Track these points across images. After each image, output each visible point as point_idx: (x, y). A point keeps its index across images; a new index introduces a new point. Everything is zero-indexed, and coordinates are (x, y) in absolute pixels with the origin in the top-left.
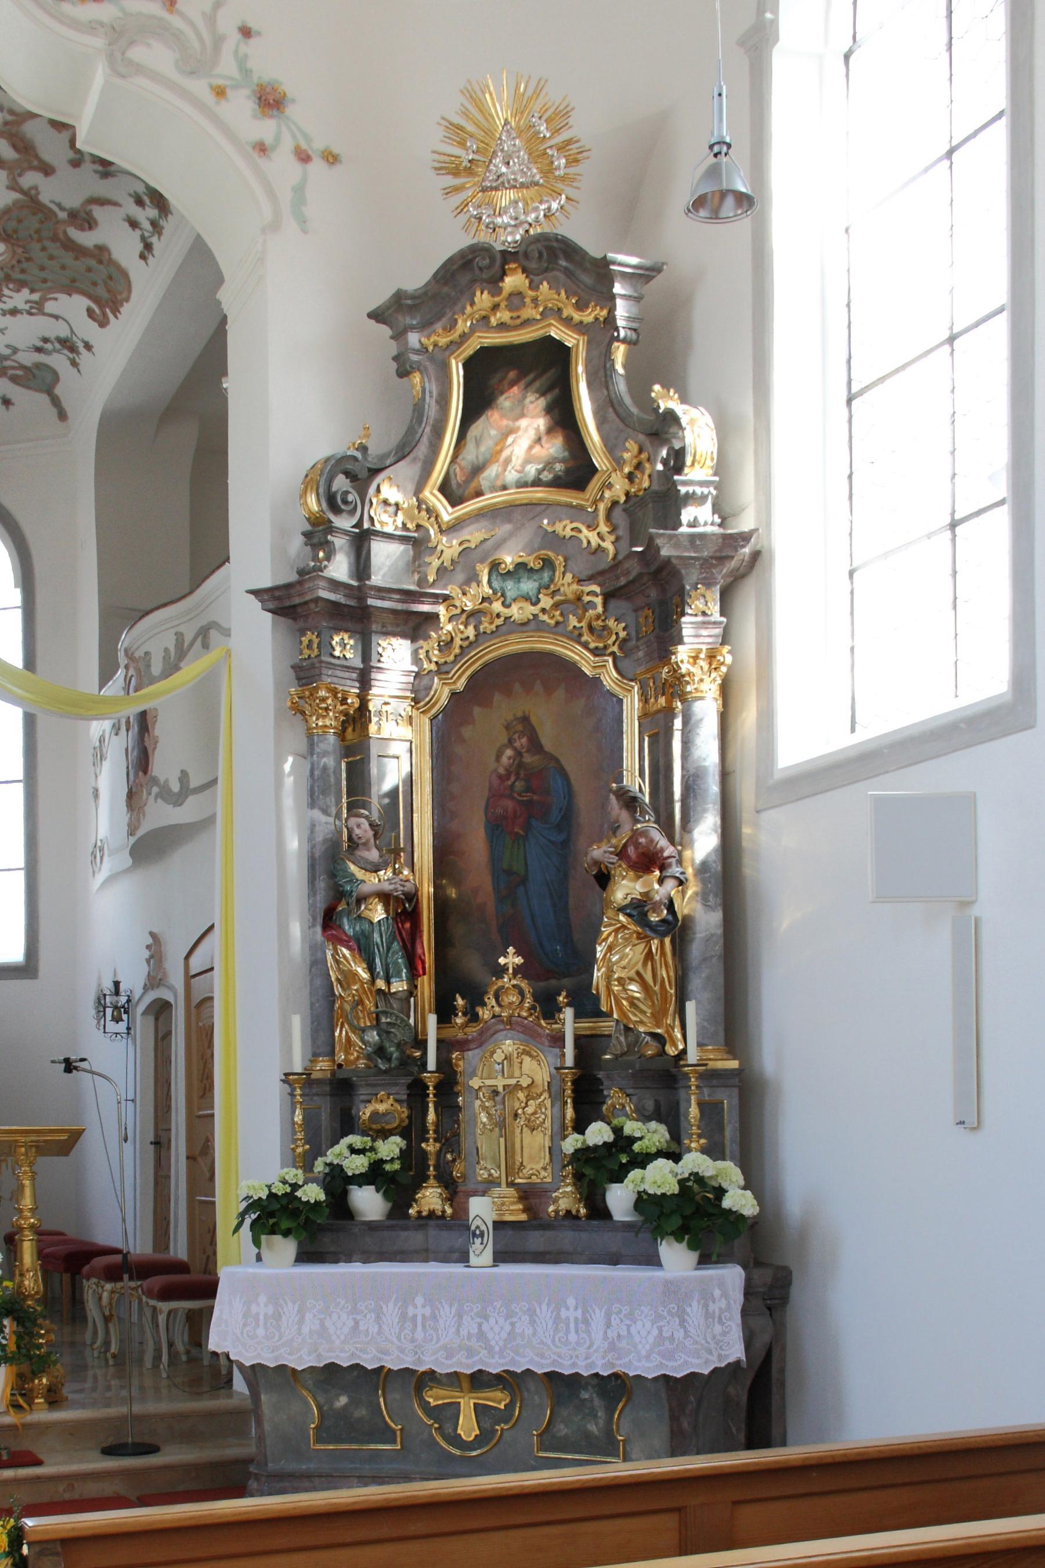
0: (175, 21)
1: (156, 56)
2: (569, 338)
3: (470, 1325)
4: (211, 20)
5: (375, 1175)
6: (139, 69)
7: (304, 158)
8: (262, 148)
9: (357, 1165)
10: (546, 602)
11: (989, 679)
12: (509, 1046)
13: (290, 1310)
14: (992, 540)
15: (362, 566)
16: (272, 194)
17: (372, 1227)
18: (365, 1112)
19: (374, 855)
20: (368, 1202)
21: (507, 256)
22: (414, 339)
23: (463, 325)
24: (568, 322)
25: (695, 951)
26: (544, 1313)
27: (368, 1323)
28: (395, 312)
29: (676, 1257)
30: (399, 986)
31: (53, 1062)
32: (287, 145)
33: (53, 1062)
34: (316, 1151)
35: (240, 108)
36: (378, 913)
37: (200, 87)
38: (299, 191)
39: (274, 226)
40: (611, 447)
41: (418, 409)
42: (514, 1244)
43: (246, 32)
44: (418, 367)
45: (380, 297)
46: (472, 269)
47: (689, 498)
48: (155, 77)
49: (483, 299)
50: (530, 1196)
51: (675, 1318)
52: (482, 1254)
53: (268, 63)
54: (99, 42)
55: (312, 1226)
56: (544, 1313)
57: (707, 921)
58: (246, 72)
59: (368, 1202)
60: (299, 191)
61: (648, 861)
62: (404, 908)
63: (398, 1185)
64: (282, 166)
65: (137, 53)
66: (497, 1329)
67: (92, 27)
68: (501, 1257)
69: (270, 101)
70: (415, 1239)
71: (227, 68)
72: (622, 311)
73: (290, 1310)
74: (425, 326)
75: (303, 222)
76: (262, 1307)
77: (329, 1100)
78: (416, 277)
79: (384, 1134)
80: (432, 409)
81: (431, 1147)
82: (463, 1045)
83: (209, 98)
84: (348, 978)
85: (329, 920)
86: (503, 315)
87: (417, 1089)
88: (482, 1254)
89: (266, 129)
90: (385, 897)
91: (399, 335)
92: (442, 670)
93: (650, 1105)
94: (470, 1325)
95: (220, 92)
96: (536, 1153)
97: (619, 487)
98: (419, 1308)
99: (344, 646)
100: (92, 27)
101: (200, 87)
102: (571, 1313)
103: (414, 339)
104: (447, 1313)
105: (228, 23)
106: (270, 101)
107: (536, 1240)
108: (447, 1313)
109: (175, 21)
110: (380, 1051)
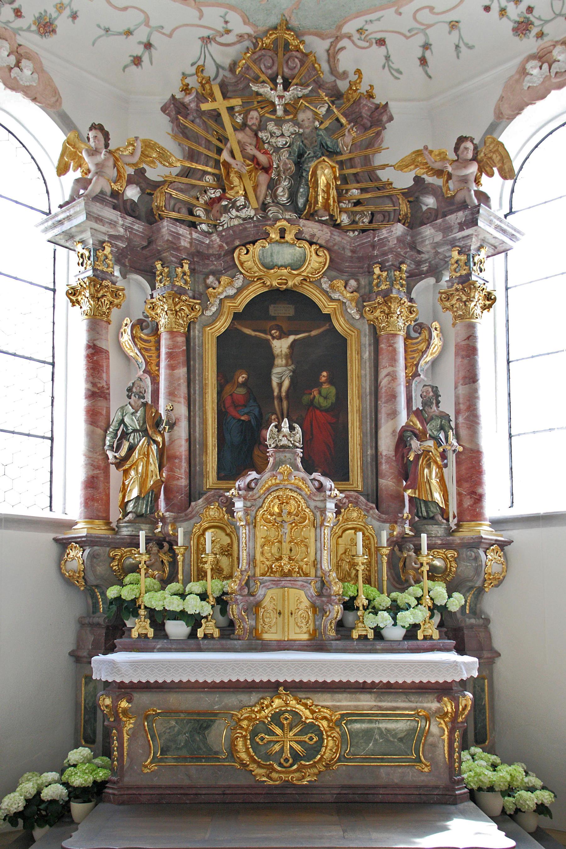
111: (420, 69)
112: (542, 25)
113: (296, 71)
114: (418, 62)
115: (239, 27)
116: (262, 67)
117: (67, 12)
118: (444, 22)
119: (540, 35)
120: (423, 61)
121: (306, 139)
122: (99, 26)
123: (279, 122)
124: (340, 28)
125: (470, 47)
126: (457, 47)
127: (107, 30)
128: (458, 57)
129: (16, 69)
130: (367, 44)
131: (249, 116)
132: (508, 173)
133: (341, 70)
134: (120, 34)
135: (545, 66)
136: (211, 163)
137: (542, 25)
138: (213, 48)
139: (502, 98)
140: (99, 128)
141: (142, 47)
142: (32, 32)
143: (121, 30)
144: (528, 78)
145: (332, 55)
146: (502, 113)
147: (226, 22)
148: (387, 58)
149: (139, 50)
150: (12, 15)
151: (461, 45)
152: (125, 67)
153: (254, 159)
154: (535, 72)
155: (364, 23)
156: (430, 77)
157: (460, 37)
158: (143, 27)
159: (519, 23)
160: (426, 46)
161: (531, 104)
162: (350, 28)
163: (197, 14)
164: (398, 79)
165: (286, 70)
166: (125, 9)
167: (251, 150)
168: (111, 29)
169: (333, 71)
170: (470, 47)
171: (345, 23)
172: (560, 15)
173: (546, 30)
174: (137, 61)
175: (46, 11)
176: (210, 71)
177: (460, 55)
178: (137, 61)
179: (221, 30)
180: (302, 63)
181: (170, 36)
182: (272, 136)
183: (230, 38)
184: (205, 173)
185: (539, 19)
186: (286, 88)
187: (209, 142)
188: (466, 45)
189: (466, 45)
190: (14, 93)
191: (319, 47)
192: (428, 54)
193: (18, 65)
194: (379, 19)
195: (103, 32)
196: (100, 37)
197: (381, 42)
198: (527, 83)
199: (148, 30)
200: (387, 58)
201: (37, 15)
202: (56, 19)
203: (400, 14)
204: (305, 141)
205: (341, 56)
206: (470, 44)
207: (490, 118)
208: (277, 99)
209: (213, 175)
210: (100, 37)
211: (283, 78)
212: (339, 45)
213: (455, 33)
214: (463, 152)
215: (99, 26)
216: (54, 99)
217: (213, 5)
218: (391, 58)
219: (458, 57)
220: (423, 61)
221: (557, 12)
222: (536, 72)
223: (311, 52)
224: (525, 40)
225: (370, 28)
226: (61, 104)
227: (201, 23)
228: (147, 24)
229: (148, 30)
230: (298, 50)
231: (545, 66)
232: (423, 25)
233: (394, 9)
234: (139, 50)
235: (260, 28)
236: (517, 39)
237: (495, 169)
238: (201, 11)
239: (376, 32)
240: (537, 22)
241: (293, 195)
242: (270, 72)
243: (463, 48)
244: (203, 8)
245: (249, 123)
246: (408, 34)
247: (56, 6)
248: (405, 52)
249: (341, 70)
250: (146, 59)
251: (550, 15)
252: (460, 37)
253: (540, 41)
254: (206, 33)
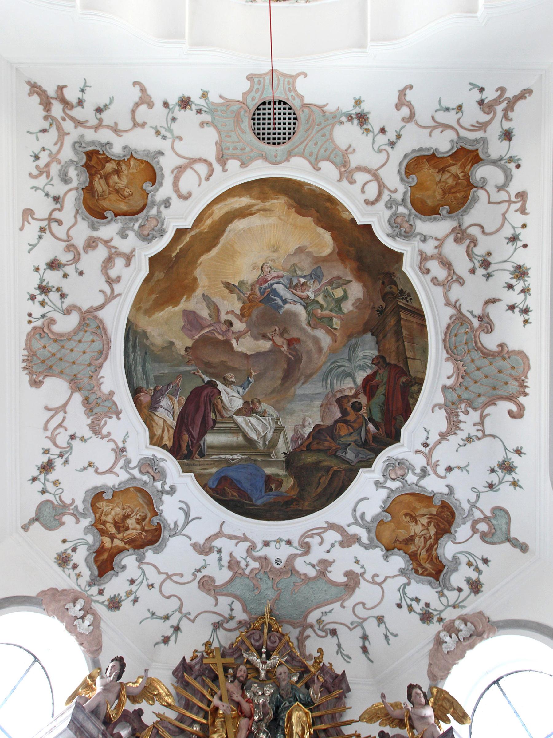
111: (363, 656)
112: (439, 614)
113: (276, 644)
114: (361, 651)
115: (240, 615)
116: (253, 641)
117: (132, 597)
118: (374, 617)
119: (440, 620)
120: (365, 650)
121: (283, 690)
122: (149, 610)
124: (306, 617)
125: (396, 635)
126: (386, 637)
127: (153, 614)
128: (388, 644)
129: (81, 620)
130: (324, 634)
131: (239, 669)
132: (462, 717)
133: (307, 653)
134: (161, 618)
135: (453, 635)
136: (202, 714)
137: (439, 614)
138: (221, 633)
139: (430, 664)
140: (120, 660)
141: (172, 629)
142: (104, 605)
143: (162, 615)
144: (444, 645)
145: (302, 640)
146: (435, 676)
147: (232, 610)
148: (339, 645)
149: (169, 632)
150: (97, 592)
151: (388, 634)
152: (157, 644)
153: (238, 705)
154: (447, 639)
155: (321, 614)
156: (372, 661)
157: (387, 629)
158: (177, 613)
159: (423, 614)
160: (365, 637)
161: (455, 664)
162: (312, 618)
163: (214, 602)
164: (349, 662)
165: (269, 643)
166: (169, 597)
167: (237, 697)
168: (157, 614)
169: (303, 654)
170: (396, 635)
171: (309, 613)
172: (448, 606)
173: (443, 615)
174: (166, 640)
175: (119, 595)
176: (215, 645)
177: (390, 642)
178: (166, 640)
179: (227, 616)
180: (280, 640)
181: (193, 621)
182: (255, 695)
183: (232, 624)
184: (194, 721)
185: (435, 610)
186: (268, 657)
187: (204, 696)
188: (392, 634)
189: (392, 634)
190: (69, 634)
191: (293, 633)
192: (367, 644)
193: (83, 618)
194: (330, 612)
195: (150, 615)
196: (148, 618)
197: (334, 632)
198: (445, 648)
199: (180, 615)
200: (339, 645)
201: (112, 596)
202: (123, 600)
203: (344, 607)
204: (282, 692)
205: (308, 643)
206: (395, 633)
208: (261, 665)
209: (201, 724)
210: (148, 618)
211: (266, 648)
212: (306, 634)
213: (382, 625)
214: (416, 697)
215: (149, 610)
216: (95, 648)
217: (225, 595)
218: (342, 646)
219: (388, 644)
220: (365, 650)
221: (446, 604)
223: (287, 634)
224: (431, 625)
225: (326, 619)
226: (99, 654)
227: (216, 610)
228: (180, 609)
229: (180, 615)
230: (278, 631)
231: (453, 635)
232: (359, 618)
233: (339, 603)
234: (169, 632)
235: (253, 616)
236: (425, 625)
237: (449, 715)
238: (217, 600)
239: (329, 623)
240: (435, 613)
242: (257, 644)
243: (390, 637)
244: (219, 597)
245: (238, 675)
246: (351, 627)
247: (126, 592)
248: (350, 641)
249: (307, 653)
250: (172, 639)
251: (443, 608)
252: (387, 629)
253: (442, 624)
254: (217, 619)
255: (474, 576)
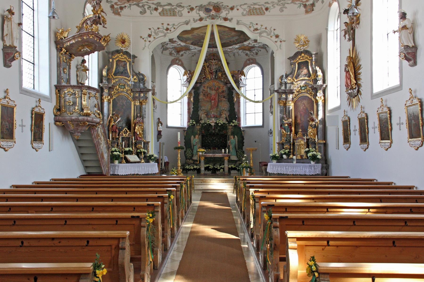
0: (266, 30)
1: (264, 34)
2: (308, 61)
3: (292, 169)
4: (270, 29)
5: (285, 154)
6: (262, 36)
7: (281, 42)
8: (276, 42)
9: (283, 152)
10: (306, 90)
11: (397, 83)
12: (300, 140)
13: (274, 167)
14: (339, 88)
15: (286, 87)
16: (277, 47)
17: (285, 159)
18: (285, 147)
19: (286, 119)
20: (285, 156)
21: (302, 52)
22: (292, 61)
23: (297, 59)
24: (308, 59)
25: (319, 130)
26: (299, 168)
27: (282, 169)
28: (290, 58)
29: (312, 163)
30: (288, 133)
31: (400, 118)
32: (279, 41)
33: (400, 118)
34: (280, 150)
35: (274, 37)
36: (286, 125)
37: (269, 37)
38: (280, 46)
39: (277, 50)
40: (313, 73)
41: (293, 69)
42: (298, 161)
43: (274, 30)
44: (292, 64)
45: (288, 57)
46: (298, 54)
47: (318, 80)
48: (264, 37)
49: (300, 57)
50: (302, 156)
51: (314, 168)
52: (295, 162)
53: (276, 33)
54: (258, 34)
55: (279, 159)
56: (299, 168)
57: (320, 126)
58: (274, 34)
59: (285, 156)
60: (280, 46)
61: (313, 120)
62: (290, 125)
63: (288, 155)
64: (279, 43)
65: (262, 35)
66: (295, 170)
67: (257, 33)
68: (297, 163)
69: (277, 36)
70: (290, 161)
71: (272, 34)
72: (313, 59)
73: (274, 167)
74: (293, 60)
75: (281, 49)
76: (272, 167)
77: (281, 145)
78: (292, 55)
79: (287, 149)
80: (294, 69)
81: (292, 151)
82: (295, 140)
83: (270, 37)
84: (283, 132)
85: (281, 126)
86: (301, 58)
87: (290, 144)
88: (295, 162)
89: (277, 40)
90: (287, 124)
91: (291, 61)
92: (295, 97)
93: (313, 146)
94: (292, 169)
95: (271, 37)
96: (303, 151)
97: (313, 78)
98: (287, 167)
99: (284, 96)
100: (257, 33)
101: (269, 37)
102: (301, 168)
103: (292, 61)
104: (290, 168)
105: (272, 29)
106: (277, 36)
107: (302, 161)
108: (290, 168)
109: (266, 30)
110: (286, 140)
123: (213, 65)
174: (193, 56)
207: (242, 66)
222: (248, 62)
241: (215, 76)
255: (257, 52)
